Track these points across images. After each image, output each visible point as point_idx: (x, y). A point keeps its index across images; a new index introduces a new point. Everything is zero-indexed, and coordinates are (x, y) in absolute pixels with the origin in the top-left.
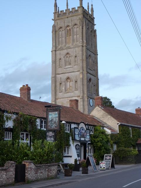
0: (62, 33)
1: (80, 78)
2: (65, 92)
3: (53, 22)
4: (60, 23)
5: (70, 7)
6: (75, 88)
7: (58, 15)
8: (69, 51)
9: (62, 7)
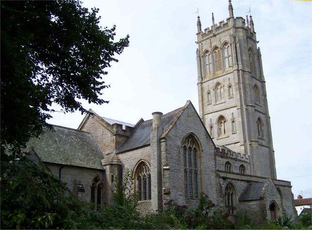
0: (209, 59)
1: (178, 147)
2: (219, 136)
3: (197, 46)
4: (206, 46)
5: (217, 22)
6: (233, 130)
7: (204, 35)
8: (220, 80)
9: (207, 24)
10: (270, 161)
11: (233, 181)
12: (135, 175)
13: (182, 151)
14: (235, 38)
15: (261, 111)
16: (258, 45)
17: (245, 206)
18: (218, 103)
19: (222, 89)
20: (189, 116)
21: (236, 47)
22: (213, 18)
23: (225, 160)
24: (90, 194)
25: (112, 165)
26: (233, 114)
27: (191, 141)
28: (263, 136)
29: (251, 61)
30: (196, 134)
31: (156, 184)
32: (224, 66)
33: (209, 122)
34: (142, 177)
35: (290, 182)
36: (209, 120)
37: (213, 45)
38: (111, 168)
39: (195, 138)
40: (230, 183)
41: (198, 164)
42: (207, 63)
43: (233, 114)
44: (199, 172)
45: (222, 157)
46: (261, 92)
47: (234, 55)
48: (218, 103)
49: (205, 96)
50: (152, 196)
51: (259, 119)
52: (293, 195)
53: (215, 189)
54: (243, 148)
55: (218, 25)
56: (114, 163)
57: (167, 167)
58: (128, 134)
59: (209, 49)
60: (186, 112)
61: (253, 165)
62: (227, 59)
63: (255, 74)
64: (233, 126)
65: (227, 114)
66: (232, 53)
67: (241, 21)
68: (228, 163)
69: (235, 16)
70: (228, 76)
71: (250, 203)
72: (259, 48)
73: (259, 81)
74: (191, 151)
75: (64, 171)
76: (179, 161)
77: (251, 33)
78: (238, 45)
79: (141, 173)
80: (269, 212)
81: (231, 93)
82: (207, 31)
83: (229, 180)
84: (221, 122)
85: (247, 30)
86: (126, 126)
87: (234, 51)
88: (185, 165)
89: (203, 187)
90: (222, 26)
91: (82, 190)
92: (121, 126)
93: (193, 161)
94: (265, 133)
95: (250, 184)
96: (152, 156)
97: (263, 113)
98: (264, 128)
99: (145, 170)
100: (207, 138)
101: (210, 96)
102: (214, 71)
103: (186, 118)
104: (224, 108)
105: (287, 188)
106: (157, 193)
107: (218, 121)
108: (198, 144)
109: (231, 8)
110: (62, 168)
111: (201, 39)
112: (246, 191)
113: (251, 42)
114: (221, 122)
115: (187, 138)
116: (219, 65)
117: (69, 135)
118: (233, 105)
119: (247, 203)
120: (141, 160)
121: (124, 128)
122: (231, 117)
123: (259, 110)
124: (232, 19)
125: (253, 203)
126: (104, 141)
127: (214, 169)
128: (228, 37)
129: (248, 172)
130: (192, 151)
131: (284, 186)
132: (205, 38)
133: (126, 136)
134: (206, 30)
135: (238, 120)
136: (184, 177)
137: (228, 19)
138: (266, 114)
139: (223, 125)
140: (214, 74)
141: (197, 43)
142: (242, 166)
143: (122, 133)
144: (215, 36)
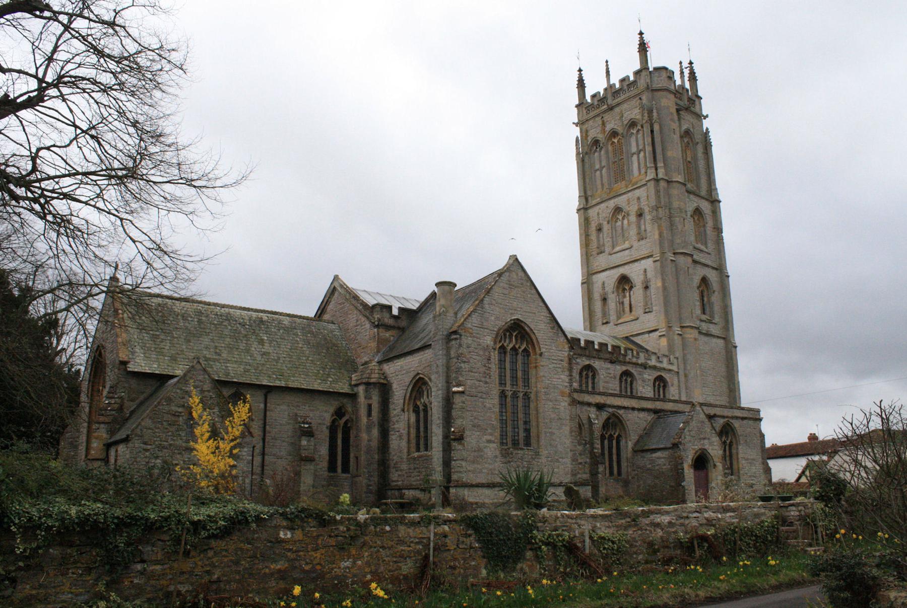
1: (486, 349)
2: (619, 318)
4: (595, 133)
5: (615, 80)
6: (646, 304)
8: (621, 201)
9: (596, 85)
10: (728, 367)
11: (621, 412)
12: (409, 404)
13: (495, 356)
14: (650, 112)
15: (710, 263)
16: (706, 124)
17: (644, 460)
18: (617, 249)
19: (626, 222)
20: (511, 286)
21: (652, 131)
22: (608, 72)
23: (619, 369)
24: (328, 439)
25: (368, 384)
26: (645, 271)
27: (516, 336)
28: (712, 316)
29: (689, 159)
30: (528, 321)
31: (440, 422)
32: (630, 171)
33: (600, 290)
34: (421, 408)
35: (758, 411)
36: (600, 286)
37: (609, 127)
38: (366, 391)
39: (525, 330)
40: (613, 415)
41: (533, 380)
42: (597, 167)
43: (645, 271)
44: (532, 396)
45: (612, 362)
46: (710, 224)
47: (649, 149)
48: (617, 249)
49: (593, 237)
50: (435, 444)
51: (704, 280)
52: (762, 436)
53: (568, 428)
54: (664, 342)
55: (617, 86)
56: (372, 380)
57: (460, 389)
58: (403, 323)
59: (601, 137)
60: (505, 278)
61: (686, 376)
62: (635, 158)
63: (698, 186)
64: (645, 297)
65: (635, 272)
66: (644, 143)
67: (664, 74)
68: (626, 373)
69: (653, 64)
70: (637, 193)
71: (654, 455)
72: (707, 129)
73: (707, 200)
74: (517, 354)
75: (273, 399)
76: (487, 374)
77: (690, 99)
78: (656, 127)
79: (420, 400)
80: (689, 473)
81: (643, 227)
82: (596, 99)
83: (610, 410)
84: (624, 289)
85: (679, 92)
86: (400, 309)
87: (648, 140)
88: (502, 383)
89: (541, 424)
90: (625, 87)
91: (309, 433)
92: (389, 308)
93: (520, 374)
94: (717, 308)
95: (659, 418)
96: (434, 368)
97: (713, 268)
98: (716, 298)
99: (425, 393)
100: (553, 328)
101: (601, 235)
102: (610, 184)
103: (506, 292)
104: (628, 259)
105: (751, 422)
106: (441, 437)
107: (618, 288)
108: (531, 340)
109: (643, 48)
110: (269, 392)
111: (585, 117)
112: (647, 433)
113: (688, 118)
114: (624, 289)
115: (507, 330)
116: (620, 172)
117: (289, 330)
118: (645, 252)
119: (648, 455)
120: (418, 374)
121: (395, 312)
122: (642, 277)
123: (703, 261)
124: (644, 73)
125: (659, 454)
126: (358, 337)
127: (567, 391)
128: (637, 111)
129: (673, 392)
130: (520, 357)
131: (743, 419)
132: (592, 114)
133: (399, 328)
134: (593, 96)
135: (656, 284)
136: (498, 406)
137: (637, 73)
138: (721, 269)
139: (627, 294)
140: (611, 189)
141: (577, 124)
142: (660, 379)
143: (391, 322)
144: (611, 108)
